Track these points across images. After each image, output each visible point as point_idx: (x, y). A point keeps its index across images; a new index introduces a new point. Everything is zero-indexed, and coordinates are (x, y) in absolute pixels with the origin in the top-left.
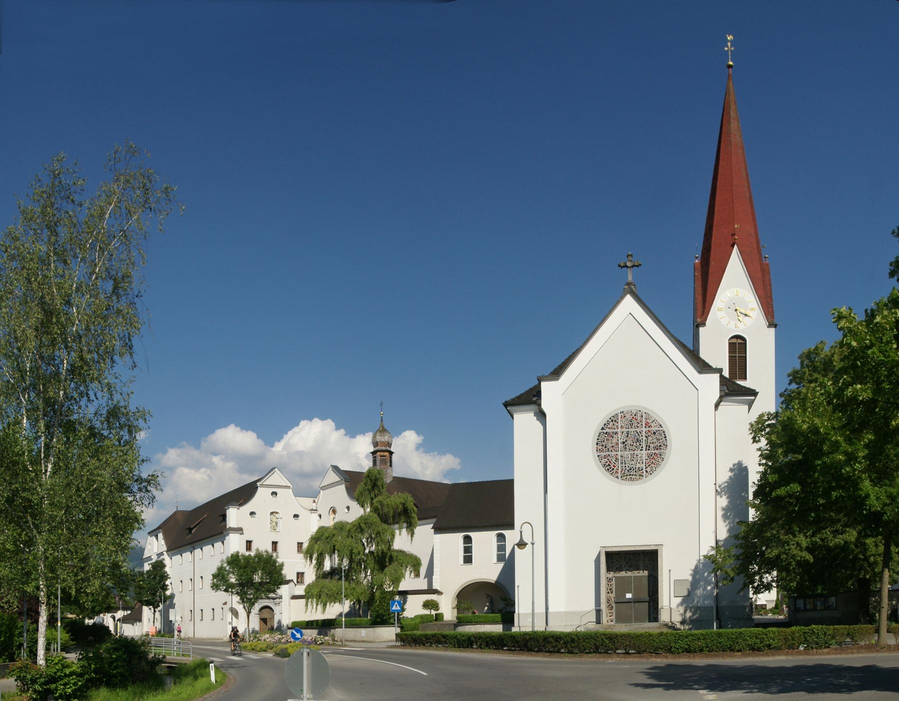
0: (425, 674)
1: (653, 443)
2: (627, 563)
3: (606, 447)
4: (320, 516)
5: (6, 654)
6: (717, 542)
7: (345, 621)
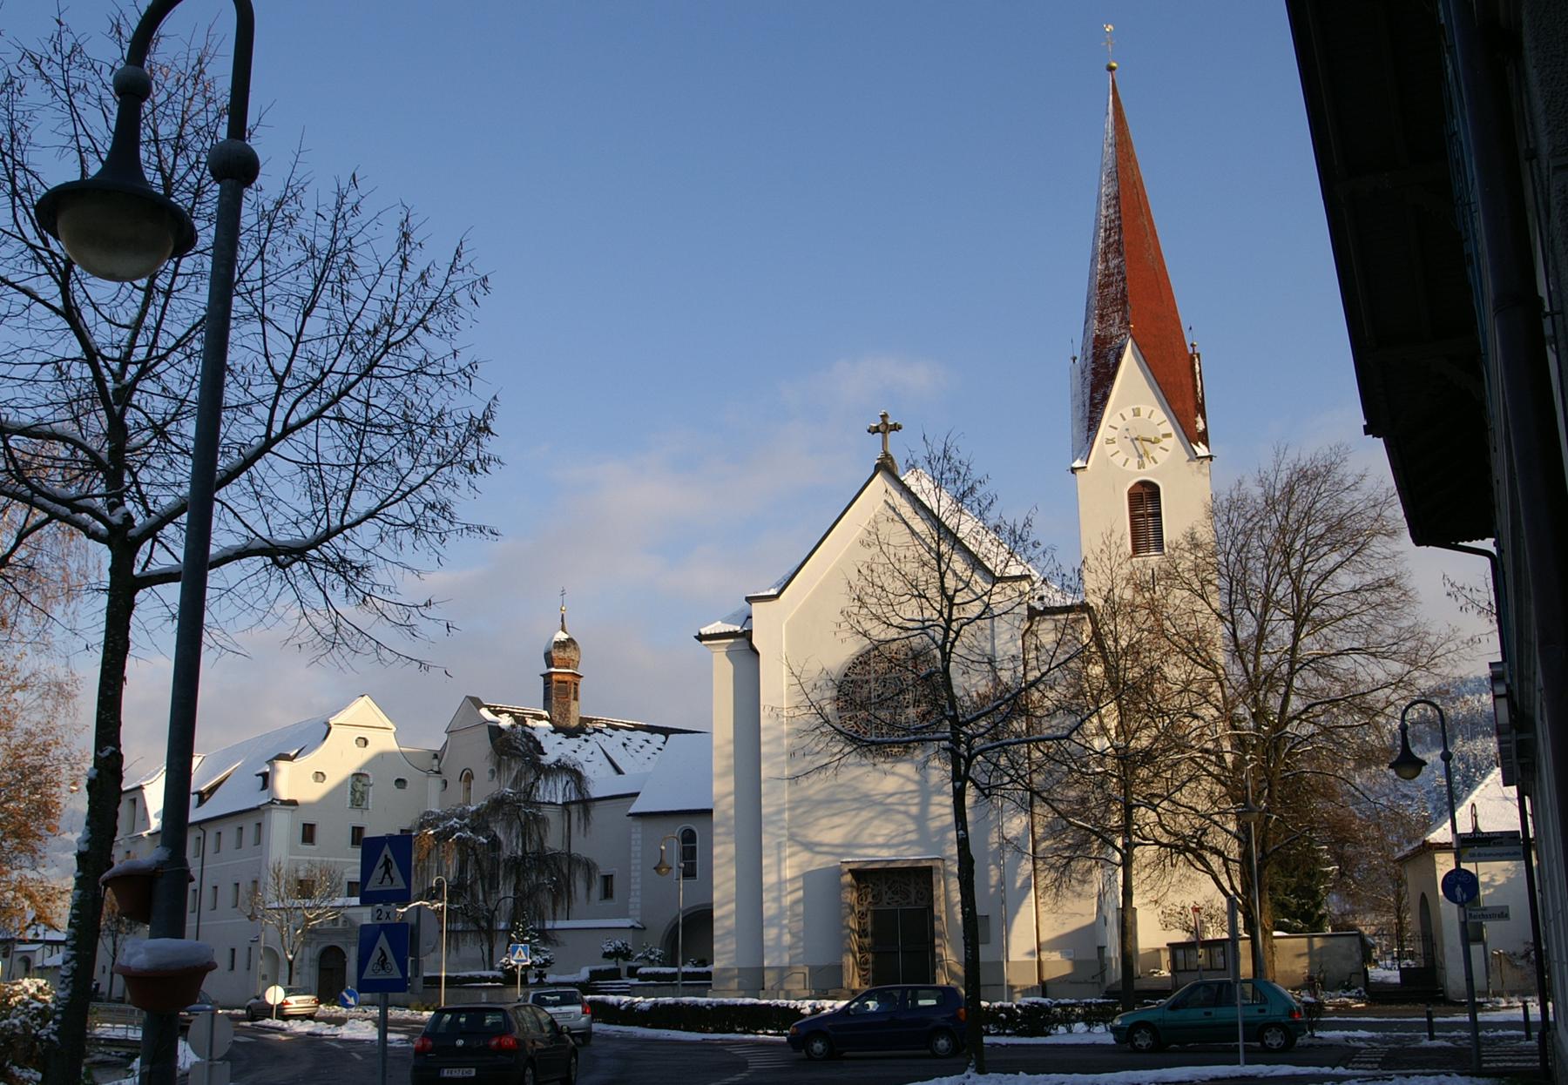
0: (446, 1073)
2: (889, 888)
4: (445, 783)
5: (990, 861)
6: (1235, 836)
7: (441, 971)
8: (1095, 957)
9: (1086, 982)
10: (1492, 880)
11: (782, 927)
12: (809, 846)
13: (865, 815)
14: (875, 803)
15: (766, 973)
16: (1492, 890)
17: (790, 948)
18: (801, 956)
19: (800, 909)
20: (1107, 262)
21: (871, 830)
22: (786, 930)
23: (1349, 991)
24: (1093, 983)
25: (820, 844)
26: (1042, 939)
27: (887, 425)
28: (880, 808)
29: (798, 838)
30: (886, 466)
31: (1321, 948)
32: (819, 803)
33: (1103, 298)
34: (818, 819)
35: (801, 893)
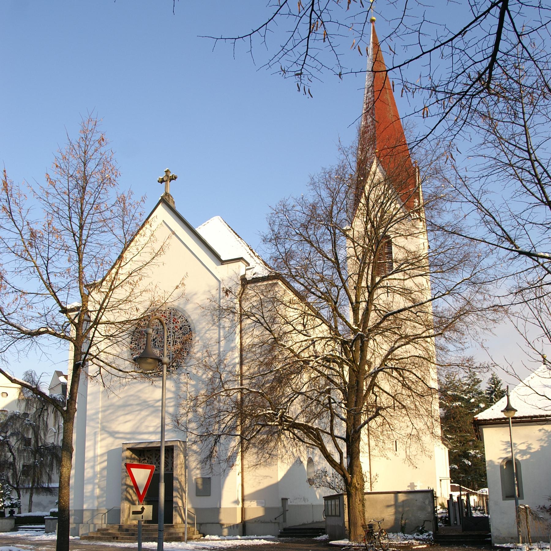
1: (179, 338)
3: (138, 345)
8: (280, 505)
9: (271, 522)
10: (529, 448)
11: (94, 484)
12: (113, 434)
13: (144, 413)
14: (150, 406)
15: (84, 512)
16: (528, 456)
17: (98, 497)
18: (105, 503)
19: (105, 473)
20: (367, 120)
21: (146, 424)
22: (97, 486)
23: (422, 533)
24: (275, 523)
25: (118, 433)
26: (247, 492)
27: (168, 176)
28: (151, 409)
29: (107, 429)
30: (166, 201)
31: (403, 501)
32: (120, 407)
33: (364, 139)
34: (118, 417)
35: (105, 464)
